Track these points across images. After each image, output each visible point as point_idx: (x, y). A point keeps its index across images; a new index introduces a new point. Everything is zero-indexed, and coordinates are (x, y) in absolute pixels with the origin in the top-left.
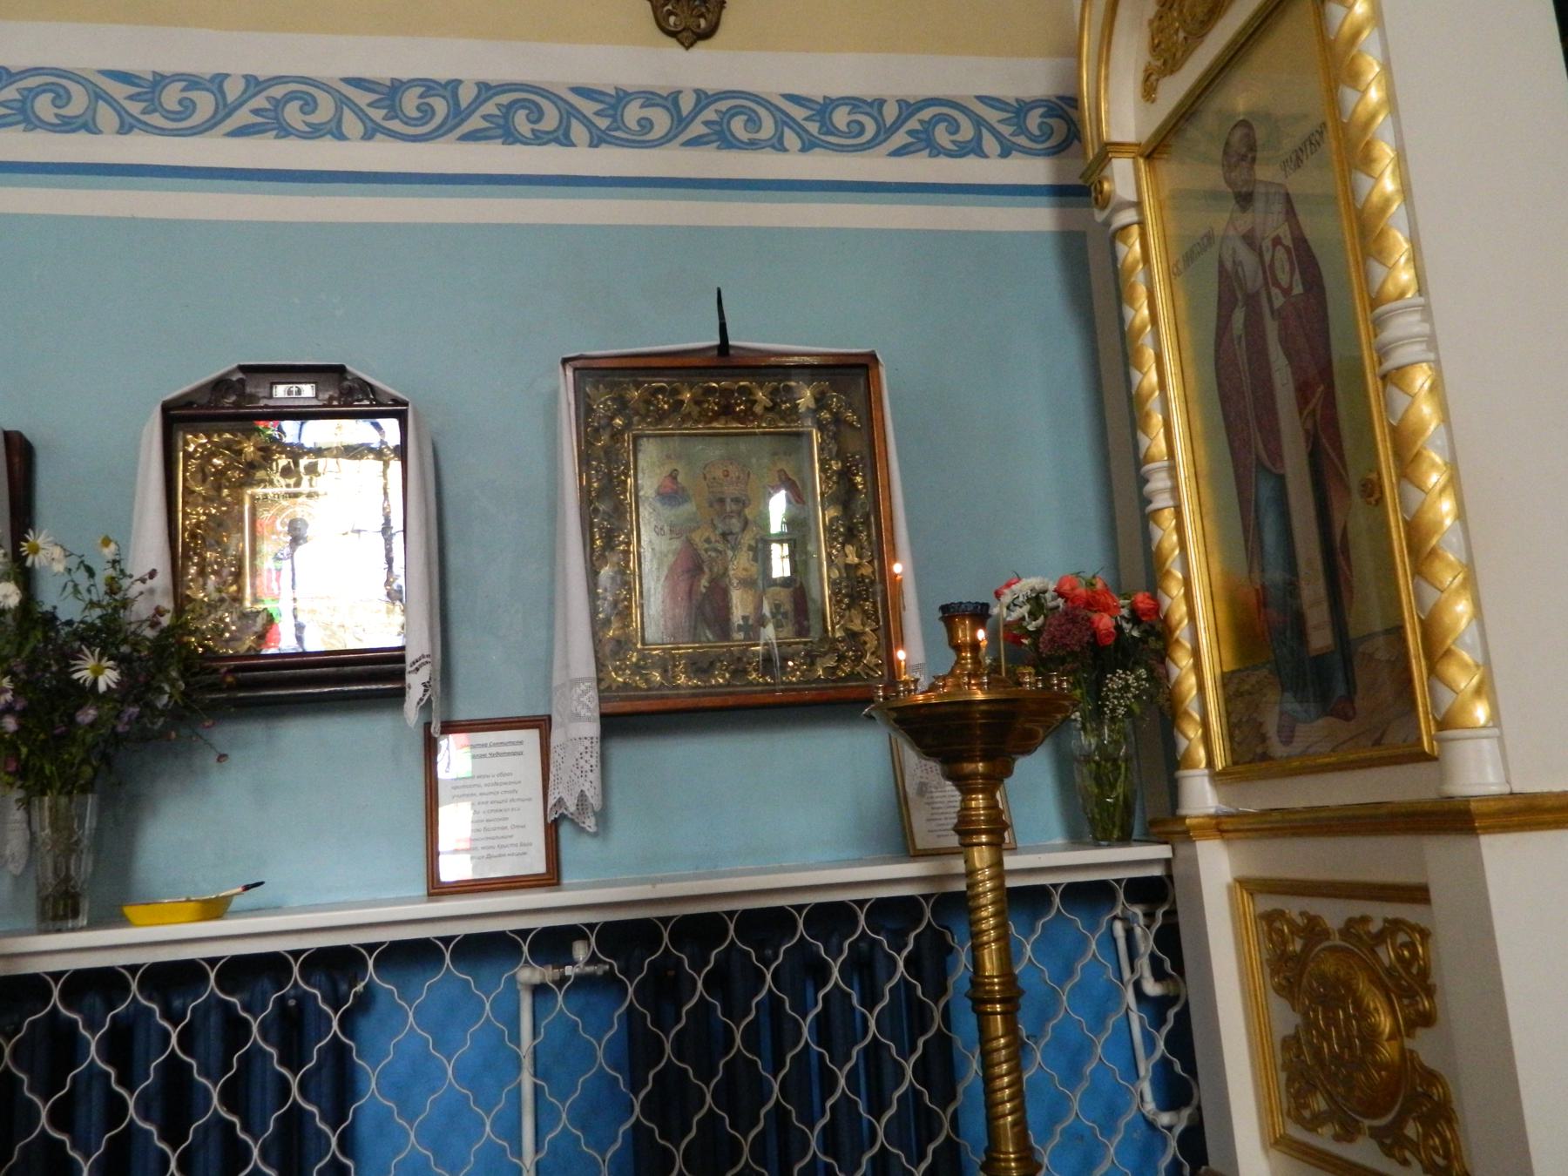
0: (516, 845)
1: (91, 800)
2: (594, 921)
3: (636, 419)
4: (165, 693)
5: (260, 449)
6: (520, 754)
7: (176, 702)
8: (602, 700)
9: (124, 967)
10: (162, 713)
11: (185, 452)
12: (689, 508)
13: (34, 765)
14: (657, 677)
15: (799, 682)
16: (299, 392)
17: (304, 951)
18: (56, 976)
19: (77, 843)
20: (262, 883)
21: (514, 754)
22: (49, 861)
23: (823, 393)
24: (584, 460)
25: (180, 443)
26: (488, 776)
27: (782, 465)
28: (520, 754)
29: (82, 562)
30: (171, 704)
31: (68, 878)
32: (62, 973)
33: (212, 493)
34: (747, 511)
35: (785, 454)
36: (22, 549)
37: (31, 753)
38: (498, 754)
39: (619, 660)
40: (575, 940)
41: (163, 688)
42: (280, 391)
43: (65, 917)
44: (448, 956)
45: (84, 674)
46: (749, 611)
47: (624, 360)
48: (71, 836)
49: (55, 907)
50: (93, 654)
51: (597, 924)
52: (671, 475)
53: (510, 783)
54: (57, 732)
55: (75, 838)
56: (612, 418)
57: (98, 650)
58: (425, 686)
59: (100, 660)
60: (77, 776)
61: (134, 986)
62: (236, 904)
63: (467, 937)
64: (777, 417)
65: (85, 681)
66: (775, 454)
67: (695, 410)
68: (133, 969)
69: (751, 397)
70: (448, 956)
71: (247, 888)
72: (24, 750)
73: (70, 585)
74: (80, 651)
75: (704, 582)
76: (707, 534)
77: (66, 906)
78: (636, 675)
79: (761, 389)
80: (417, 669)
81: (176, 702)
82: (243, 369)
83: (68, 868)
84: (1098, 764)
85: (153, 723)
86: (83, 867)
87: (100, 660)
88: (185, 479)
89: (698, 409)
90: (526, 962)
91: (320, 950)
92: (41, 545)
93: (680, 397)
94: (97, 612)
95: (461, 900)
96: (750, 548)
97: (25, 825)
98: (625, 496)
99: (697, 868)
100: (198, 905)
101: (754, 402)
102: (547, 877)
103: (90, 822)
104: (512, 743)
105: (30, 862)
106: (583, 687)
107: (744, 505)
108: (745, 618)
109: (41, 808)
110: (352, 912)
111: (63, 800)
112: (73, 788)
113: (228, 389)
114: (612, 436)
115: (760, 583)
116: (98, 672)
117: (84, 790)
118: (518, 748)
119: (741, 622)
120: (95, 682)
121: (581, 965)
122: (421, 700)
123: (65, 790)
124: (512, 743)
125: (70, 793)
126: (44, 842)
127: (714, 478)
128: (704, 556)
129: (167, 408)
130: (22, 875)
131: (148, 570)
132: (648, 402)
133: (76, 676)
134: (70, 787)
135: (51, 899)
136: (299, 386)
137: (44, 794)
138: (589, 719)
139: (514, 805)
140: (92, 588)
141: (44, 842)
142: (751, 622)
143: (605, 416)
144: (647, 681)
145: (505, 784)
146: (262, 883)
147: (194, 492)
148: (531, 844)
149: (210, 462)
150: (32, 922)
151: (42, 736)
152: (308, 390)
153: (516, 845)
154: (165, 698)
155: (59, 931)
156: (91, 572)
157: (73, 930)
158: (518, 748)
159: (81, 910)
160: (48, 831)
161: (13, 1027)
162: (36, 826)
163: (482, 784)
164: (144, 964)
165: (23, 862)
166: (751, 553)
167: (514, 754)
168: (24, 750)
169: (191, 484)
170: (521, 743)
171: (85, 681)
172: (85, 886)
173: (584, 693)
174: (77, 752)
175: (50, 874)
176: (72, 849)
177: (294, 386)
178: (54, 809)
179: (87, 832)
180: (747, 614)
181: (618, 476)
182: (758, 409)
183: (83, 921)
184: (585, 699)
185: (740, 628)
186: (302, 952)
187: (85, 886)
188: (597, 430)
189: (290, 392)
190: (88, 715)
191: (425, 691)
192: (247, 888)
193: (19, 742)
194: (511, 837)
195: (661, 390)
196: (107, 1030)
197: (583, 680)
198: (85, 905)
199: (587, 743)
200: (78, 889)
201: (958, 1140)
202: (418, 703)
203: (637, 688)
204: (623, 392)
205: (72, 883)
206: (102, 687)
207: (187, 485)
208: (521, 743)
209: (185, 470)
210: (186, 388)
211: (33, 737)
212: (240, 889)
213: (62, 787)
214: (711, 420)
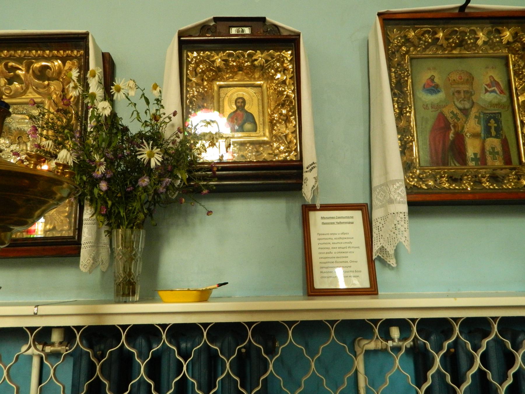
0: (353, 272)
1: (142, 232)
2: (415, 317)
3: (412, 49)
4: (179, 179)
5: (223, 60)
6: (353, 223)
7: (184, 184)
8: (408, 194)
9: (159, 325)
10: (178, 189)
11: (187, 60)
12: (441, 96)
13: (115, 211)
14: (431, 183)
15: (513, 188)
16: (243, 31)
17: (254, 323)
18: (124, 327)
19: (135, 255)
20: (227, 283)
21: (349, 223)
22: (121, 264)
23: (516, 34)
24: (389, 67)
25: (185, 55)
26: (336, 234)
27: (491, 74)
28: (353, 223)
29: (143, 94)
30: (182, 185)
31: (130, 274)
32: (127, 326)
33: (200, 82)
34: (473, 97)
35: (493, 68)
36: (111, 91)
37: (113, 204)
38: (340, 223)
39: (411, 173)
40: (393, 326)
41: (178, 176)
42: (234, 31)
43: (128, 295)
44: (333, 332)
45: (144, 157)
46: (478, 150)
47: (411, 15)
48: (132, 251)
49: (124, 289)
50: (148, 144)
51: (417, 319)
52: (430, 78)
53: (348, 238)
54: (128, 190)
55: (134, 252)
56: (401, 47)
57: (151, 142)
58: (315, 179)
59: (152, 148)
60: (136, 218)
61: (164, 336)
62: (214, 293)
63: (344, 321)
64: (489, 48)
65: (144, 160)
66: (487, 68)
67: (445, 43)
68: (164, 326)
69: (476, 36)
70: (333, 332)
71: (220, 285)
72: (110, 203)
73: (135, 113)
74: (143, 143)
75: (451, 135)
76: (452, 110)
77: (129, 289)
78: (420, 181)
79: (482, 31)
80: (311, 170)
81: (184, 184)
82: (216, 19)
83: (130, 269)
84: (123, 283)
85: (172, 196)
86: (137, 269)
87: (152, 148)
88: (187, 74)
89: (447, 42)
90: (377, 338)
91: (263, 323)
92: (122, 87)
93: (437, 36)
94: (148, 129)
95: (321, 300)
96: (476, 117)
97: (108, 246)
98: (407, 88)
99: (449, 290)
100: (199, 293)
101: (478, 38)
102: (370, 290)
103: (141, 245)
104: (348, 217)
105: (111, 264)
106: (398, 185)
107: (472, 95)
108: (475, 154)
109: (117, 236)
110: (281, 302)
111: (129, 231)
112: (134, 225)
113: (208, 29)
114: (401, 56)
115: (482, 135)
116: (151, 155)
117: (139, 227)
118: (351, 220)
119: (473, 156)
120: (149, 162)
121: (396, 340)
122: (314, 186)
123: (130, 226)
124: (348, 217)
125: (132, 228)
126: (118, 254)
127: (454, 80)
128: (450, 120)
129: (181, 34)
130: (106, 271)
131: (173, 111)
132: (420, 39)
133: (139, 157)
134: (132, 225)
135: (121, 285)
136: (242, 28)
137: (118, 227)
138: (403, 203)
139: (352, 250)
140: (148, 111)
141: (118, 254)
142: (478, 156)
143: (397, 46)
144: (427, 185)
145: (326, 244)
146: (227, 283)
147: (191, 80)
148: (360, 271)
149: (198, 66)
150: (112, 297)
151: (119, 195)
152: (247, 31)
153: (353, 272)
154: (179, 182)
155: (125, 302)
156: (148, 102)
157: (133, 302)
158: (351, 220)
159: (136, 291)
160: (120, 247)
161: (100, 352)
162: (114, 246)
163: (334, 238)
164: (169, 324)
165: (107, 265)
166: (477, 120)
167: (349, 223)
168: (110, 203)
169: (190, 76)
170: (352, 217)
171: (144, 160)
172: (139, 279)
173: (399, 187)
174: (136, 205)
175: (121, 272)
176: (131, 258)
177: (240, 28)
178: (124, 238)
179: (140, 250)
180: (476, 152)
181: (404, 78)
182: (480, 42)
183: (137, 298)
184: (399, 191)
185: (473, 160)
186: (253, 323)
187: (139, 279)
188: (393, 53)
189: (238, 31)
190: (144, 181)
191: (316, 182)
192: (220, 285)
193: (107, 199)
194: (350, 267)
195: (428, 32)
196: (150, 359)
197: (397, 181)
198: (138, 289)
199: (402, 215)
200: (135, 280)
201: (365, 376)
202: (312, 188)
203: (421, 188)
204: (407, 34)
205: (132, 277)
206: (153, 165)
207: (188, 76)
208: (352, 217)
209: (187, 69)
210: (190, 25)
211: (115, 195)
212: (216, 286)
213: (128, 224)
214: (454, 48)
